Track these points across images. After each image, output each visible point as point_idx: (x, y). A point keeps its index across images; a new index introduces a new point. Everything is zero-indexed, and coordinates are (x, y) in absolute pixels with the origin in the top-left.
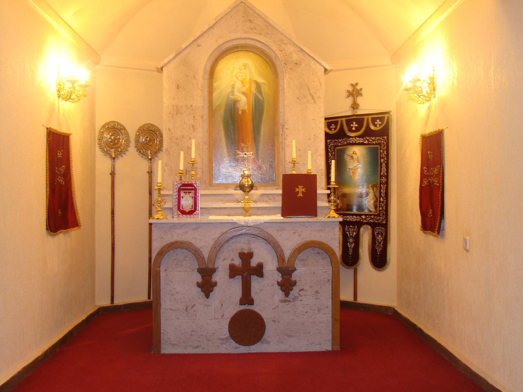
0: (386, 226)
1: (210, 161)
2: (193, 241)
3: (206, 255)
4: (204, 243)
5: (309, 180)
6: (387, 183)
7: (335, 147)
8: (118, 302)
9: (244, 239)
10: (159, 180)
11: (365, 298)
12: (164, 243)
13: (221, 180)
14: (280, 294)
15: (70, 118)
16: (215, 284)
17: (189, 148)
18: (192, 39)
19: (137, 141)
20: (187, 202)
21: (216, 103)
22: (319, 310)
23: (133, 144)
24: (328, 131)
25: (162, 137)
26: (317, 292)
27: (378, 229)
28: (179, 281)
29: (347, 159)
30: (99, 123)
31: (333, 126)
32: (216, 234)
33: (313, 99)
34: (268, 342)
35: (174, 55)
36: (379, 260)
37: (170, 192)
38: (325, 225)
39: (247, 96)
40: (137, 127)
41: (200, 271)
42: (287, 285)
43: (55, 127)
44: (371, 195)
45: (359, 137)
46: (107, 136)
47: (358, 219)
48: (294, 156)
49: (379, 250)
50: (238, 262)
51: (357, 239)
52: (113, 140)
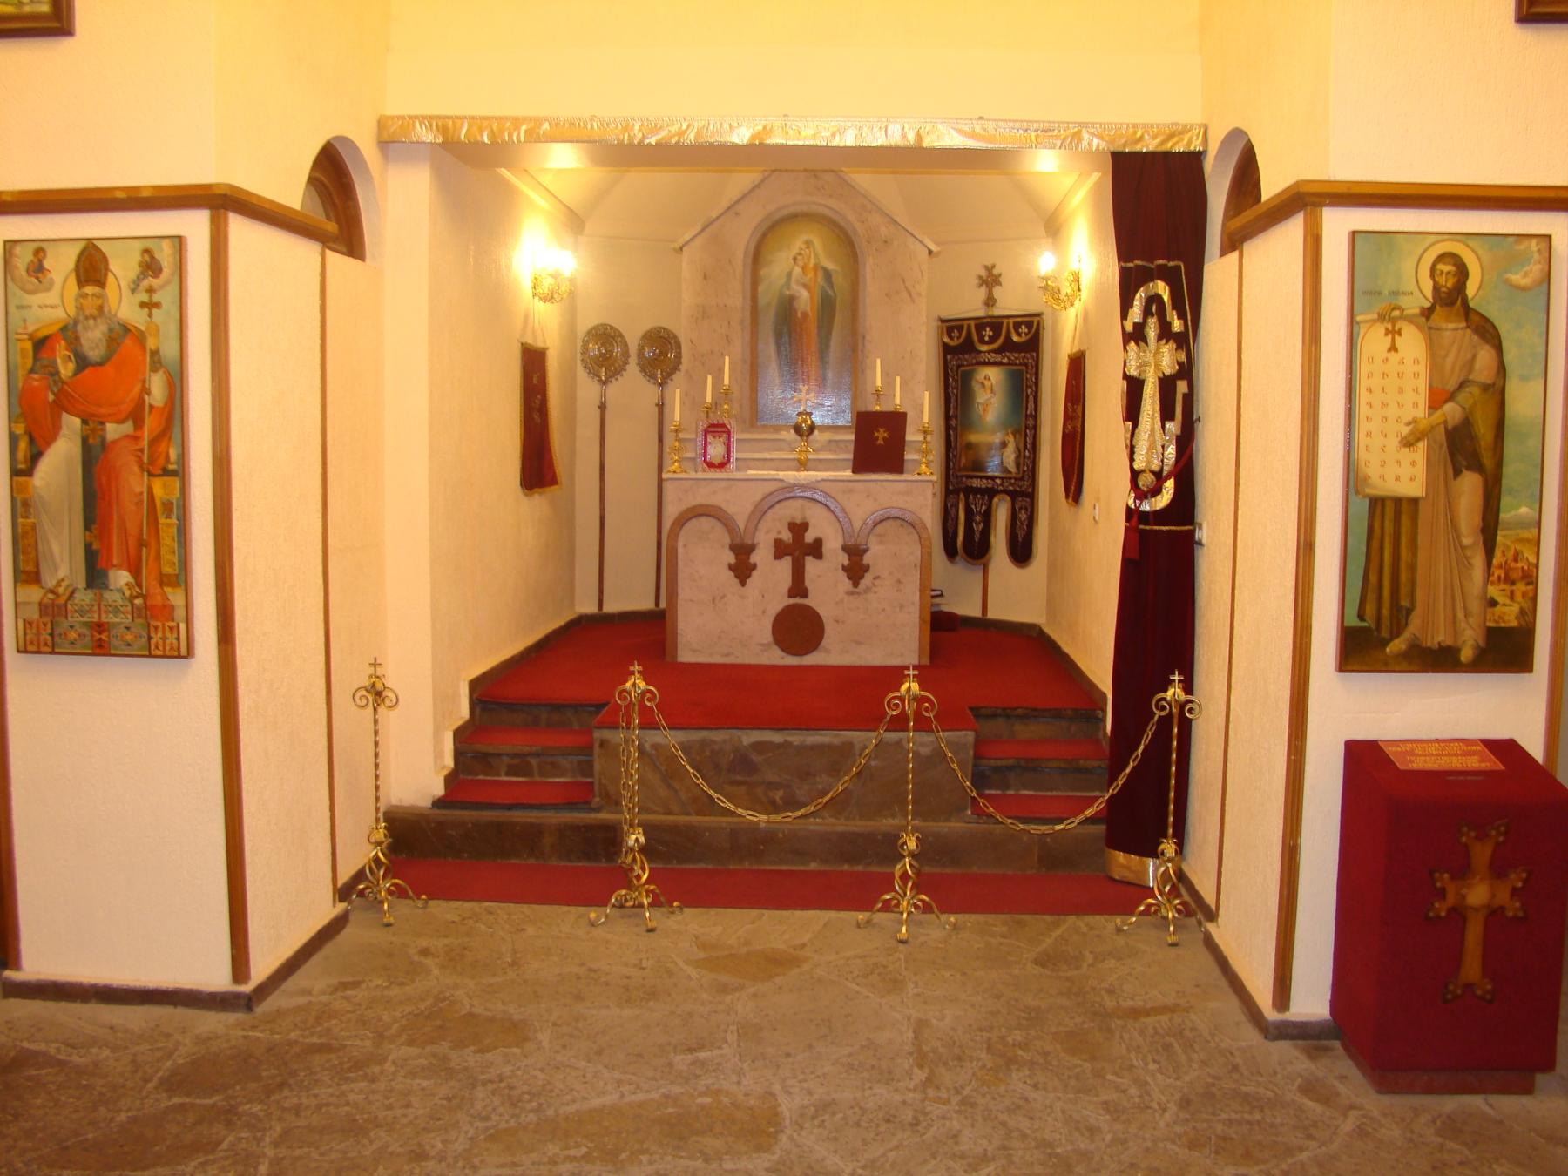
0: (1031, 496)
1: (754, 389)
2: (723, 506)
3: (742, 526)
4: (739, 507)
5: (896, 421)
6: (1035, 428)
7: (959, 366)
8: (609, 608)
10: (677, 417)
12: (683, 507)
14: (847, 584)
15: (547, 325)
16: (754, 567)
17: (721, 370)
18: (724, 204)
19: (640, 354)
20: (716, 450)
21: (763, 300)
22: (901, 607)
23: (633, 360)
24: (946, 340)
25: (679, 346)
28: (704, 560)
29: (976, 387)
32: (757, 493)
33: (910, 294)
34: (827, 651)
35: (699, 228)
36: (1021, 552)
38: (917, 489)
40: (640, 334)
41: (734, 548)
42: (856, 569)
43: (529, 340)
45: (995, 351)
46: (595, 350)
47: (990, 484)
48: (879, 383)
49: (1021, 534)
50: (786, 536)
51: (987, 517)
52: (604, 351)
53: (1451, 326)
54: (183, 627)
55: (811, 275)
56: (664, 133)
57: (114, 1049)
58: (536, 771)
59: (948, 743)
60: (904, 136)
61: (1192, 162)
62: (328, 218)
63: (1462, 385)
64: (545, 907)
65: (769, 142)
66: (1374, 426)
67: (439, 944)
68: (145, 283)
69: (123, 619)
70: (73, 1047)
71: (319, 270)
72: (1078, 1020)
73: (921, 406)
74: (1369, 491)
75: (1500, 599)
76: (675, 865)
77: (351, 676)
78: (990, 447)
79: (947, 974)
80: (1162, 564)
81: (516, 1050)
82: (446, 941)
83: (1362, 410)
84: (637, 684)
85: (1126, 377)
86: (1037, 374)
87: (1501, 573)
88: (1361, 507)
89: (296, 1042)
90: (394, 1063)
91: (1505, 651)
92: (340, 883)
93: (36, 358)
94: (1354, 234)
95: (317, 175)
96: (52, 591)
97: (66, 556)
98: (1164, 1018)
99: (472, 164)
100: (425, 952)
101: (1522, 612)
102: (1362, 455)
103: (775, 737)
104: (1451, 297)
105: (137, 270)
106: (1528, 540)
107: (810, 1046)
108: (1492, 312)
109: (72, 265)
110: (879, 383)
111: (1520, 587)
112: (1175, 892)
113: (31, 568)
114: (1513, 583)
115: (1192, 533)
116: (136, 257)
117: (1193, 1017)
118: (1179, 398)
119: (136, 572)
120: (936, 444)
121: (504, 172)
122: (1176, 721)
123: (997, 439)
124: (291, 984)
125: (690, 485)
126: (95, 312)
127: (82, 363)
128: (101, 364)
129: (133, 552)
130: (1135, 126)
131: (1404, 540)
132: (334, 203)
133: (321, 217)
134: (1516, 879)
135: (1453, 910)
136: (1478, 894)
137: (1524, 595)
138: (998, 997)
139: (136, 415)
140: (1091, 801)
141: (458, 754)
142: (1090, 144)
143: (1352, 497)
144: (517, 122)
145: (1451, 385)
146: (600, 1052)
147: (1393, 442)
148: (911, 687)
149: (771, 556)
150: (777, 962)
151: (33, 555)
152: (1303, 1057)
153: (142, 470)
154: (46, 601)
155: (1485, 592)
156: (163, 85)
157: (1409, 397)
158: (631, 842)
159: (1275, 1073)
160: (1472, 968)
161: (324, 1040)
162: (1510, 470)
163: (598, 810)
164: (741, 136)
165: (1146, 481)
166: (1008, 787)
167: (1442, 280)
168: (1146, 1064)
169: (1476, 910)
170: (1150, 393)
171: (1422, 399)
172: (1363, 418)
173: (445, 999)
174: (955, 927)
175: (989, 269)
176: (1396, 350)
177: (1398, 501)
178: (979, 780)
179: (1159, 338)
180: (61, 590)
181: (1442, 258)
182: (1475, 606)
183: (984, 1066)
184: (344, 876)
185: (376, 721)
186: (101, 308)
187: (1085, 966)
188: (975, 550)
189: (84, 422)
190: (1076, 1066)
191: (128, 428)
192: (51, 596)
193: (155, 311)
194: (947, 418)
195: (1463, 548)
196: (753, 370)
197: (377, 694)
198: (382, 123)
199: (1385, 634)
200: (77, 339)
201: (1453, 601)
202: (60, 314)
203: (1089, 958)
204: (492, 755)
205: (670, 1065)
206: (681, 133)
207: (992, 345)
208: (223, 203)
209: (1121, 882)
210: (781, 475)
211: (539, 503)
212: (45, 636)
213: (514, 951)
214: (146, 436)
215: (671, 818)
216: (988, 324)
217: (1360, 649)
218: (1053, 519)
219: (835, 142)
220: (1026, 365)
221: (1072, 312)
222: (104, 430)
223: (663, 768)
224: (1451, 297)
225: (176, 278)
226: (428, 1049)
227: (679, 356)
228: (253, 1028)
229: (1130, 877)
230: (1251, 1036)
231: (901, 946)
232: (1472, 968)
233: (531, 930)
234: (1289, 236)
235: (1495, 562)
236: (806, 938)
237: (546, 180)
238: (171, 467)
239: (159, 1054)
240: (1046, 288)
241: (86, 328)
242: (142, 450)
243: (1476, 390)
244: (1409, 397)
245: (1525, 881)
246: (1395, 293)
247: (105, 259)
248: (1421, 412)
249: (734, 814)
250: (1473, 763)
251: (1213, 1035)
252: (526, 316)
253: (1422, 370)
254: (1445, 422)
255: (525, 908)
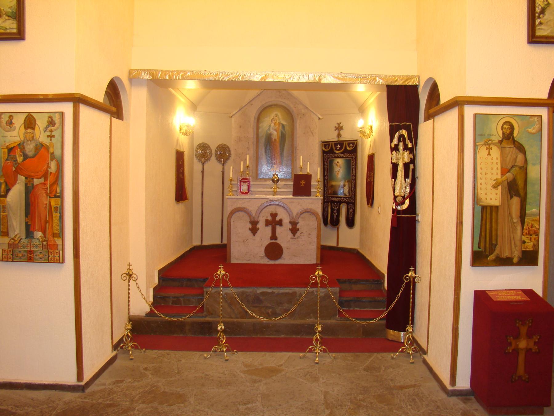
0: (354, 204)
1: (257, 166)
2: (247, 207)
3: (254, 214)
4: (253, 208)
5: (308, 178)
6: (355, 180)
7: (328, 158)
8: (205, 243)
9: (273, 207)
11: (343, 244)
13: (262, 176)
14: (290, 235)
15: (184, 143)
16: (258, 229)
17: (246, 159)
19: (216, 153)
20: (244, 188)
21: (260, 135)
22: (310, 243)
23: (214, 155)
24: (324, 149)
25: (230, 151)
26: (309, 234)
27: (350, 206)
28: (240, 227)
29: (334, 166)
30: (196, 143)
31: (327, 147)
34: (284, 259)
36: (351, 223)
37: (236, 183)
38: (315, 201)
39: (277, 131)
42: (294, 230)
44: (347, 187)
45: (341, 153)
46: (200, 151)
47: (339, 199)
48: (301, 164)
49: (350, 217)
50: (270, 218)
51: (339, 211)
52: (203, 153)
53: (509, 146)
54: (61, 252)
55: (277, 126)
56: (230, 76)
57: (34, 407)
58: (182, 302)
59: (332, 292)
60: (315, 79)
61: (415, 88)
62: (111, 105)
63: (513, 167)
64: (188, 352)
65: (267, 80)
66: (483, 181)
67: (150, 366)
68: (49, 129)
69: (39, 249)
70: (18, 407)
71: (109, 124)
72: (381, 391)
73: (315, 170)
74: (481, 204)
75: (527, 241)
76: (233, 336)
77: (119, 269)
78: (339, 186)
79: (334, 375)
80: (405, 229)
81: (182, 405)
82: (153, 365)
83: (479, 175)
84: (221, 272)
85: (392, 163)
86: (356, 161)
87: (527, 232)
88: (479, 209)
89: (101, 403)
90: (138, 410)
91: (529, 259)
92: (114, 344)
93: (8, 155)
94: (475, 115)
95: (109, 91)
96: (13, 239)
97: (18, 226)
98: (412, 389)
99: (160, 86)
100: (146, 369)
101: (534, 245)
102: (479, 191)
103: (269, 290)
104: (509, 136)
105: (47, 124)
106: (536, 220)
107: (287, 402)
108: (523, 142)
109: (23, 122)
110: (301, 164)
111: (533, 236)
112: (411, 344)
113: (5, 230)
114: (531, 235)
115: (415, 217)
116: (46, 119)
117: (422, 389)
118: (410, 171)
119: (44, 233)
120: (321, 185)
121: (171, 90)
122: (412, 283)
123: (342, 184)
124: (97, 381)
125: (234, 200)
126: (31, 139)
127: (26, 157)
128: (33, 157)
129: (43, 225)
130: (394, 76)
131: (494, 220)
132: (113, 101)
133: (108, 103)
134: (536, 338)
135: (513, 350)
136: (523, 344)
137: (535, 239)
138: (352, 383)
139: (45, 176)
140: (382, 312)
141: (155, 297)
142: (379, 81)
143: (476, 206)
144: (178, 72)
145: (509, 167)
146: (212, 405)
147: (489, 187)
148: (319, 273)
149: (264, 225)
150: (273, 371)
151: (6, 226)
152: (461, 402)
153: (47, 195)
154: (10, 242)
155: (521, 238)
156: (56, 57)
157: (494, 171)
158: (219, 328)
159: (452, 409)
160: (521, 370)
161: (111, 402)
162: (529, 196)
163: (205, 317)
164: (257, 78)
165: (399, 199)
166: (351, 307)
167: (505, 131)
168: (407, 406)
169: (522, 349)
170: (401, 169)
171: (499, 171)
172: (479, 179)
173: (154, 386)
174: (335, 357)
175: (339, 124)
176: (490, 155)
177: (491, 207)
178: (341, 303)
179: (404, 150)
180: (16, 239)
181: (505, 123)
182: (518, 243)
183: (350, 408)
184: (116, 341)
185: (129, 285)
186: (33, 137)
187: (382, 371)
188: (335, 223)
189: (26, 178)
190: (382, 407)
191: (42, 180)
192: (12, 241)
193: (53, 138)
194: (324, 176)
195: (514, 223)
196: (257, 160)
197: (130, 275)
198: (130, 72)
199: (487, 253)
200: (24, 148)
201: (511, 241)
202: (18, 139)
203: (383, 368)
204: (167, 297)
205: (238, 409)
206: (236, 77)
207: (340, 150)
208: (78, 100)
209: (392, 341)
210: (268, 197)
211: (181, 206)
212: (10, 255)
213: (178, 369)
214: (48, 183)
215: (232, 319)
216: (338, 144)
217: (478, 259)
218: (362, 212)
219: (289, 81)
220: (352, 158)
221: (369, 140)
222: (33, 181)
223: (229, 301)
224: (509, 136)
225: (61, 127)
226: (150, 405)
227: (230, 154)
228: (85, 398)
229: (395, 339)
230: (443, 395)
231: (316, 365)
232: (521, 370)
233: (183, 361)
234: (452, 115)
235: (525, 228)
236: (282, 362)
237: (185, 92)
238: (57, 195)
239: (51, 409)
240: (360, 132)
241: (27, 144)
242: (47, 188)
243: (517, 169)
244: (494, 171)
245: (539, 339)
246: (489, 135)
247: (35, 120)
248: (499, 176)
249: (255, 318)
250: (519, 298)
251: (429, 395)
252: (178, 140)
253: (499, 161)
254: (507, 180)
255: (181, 353)
